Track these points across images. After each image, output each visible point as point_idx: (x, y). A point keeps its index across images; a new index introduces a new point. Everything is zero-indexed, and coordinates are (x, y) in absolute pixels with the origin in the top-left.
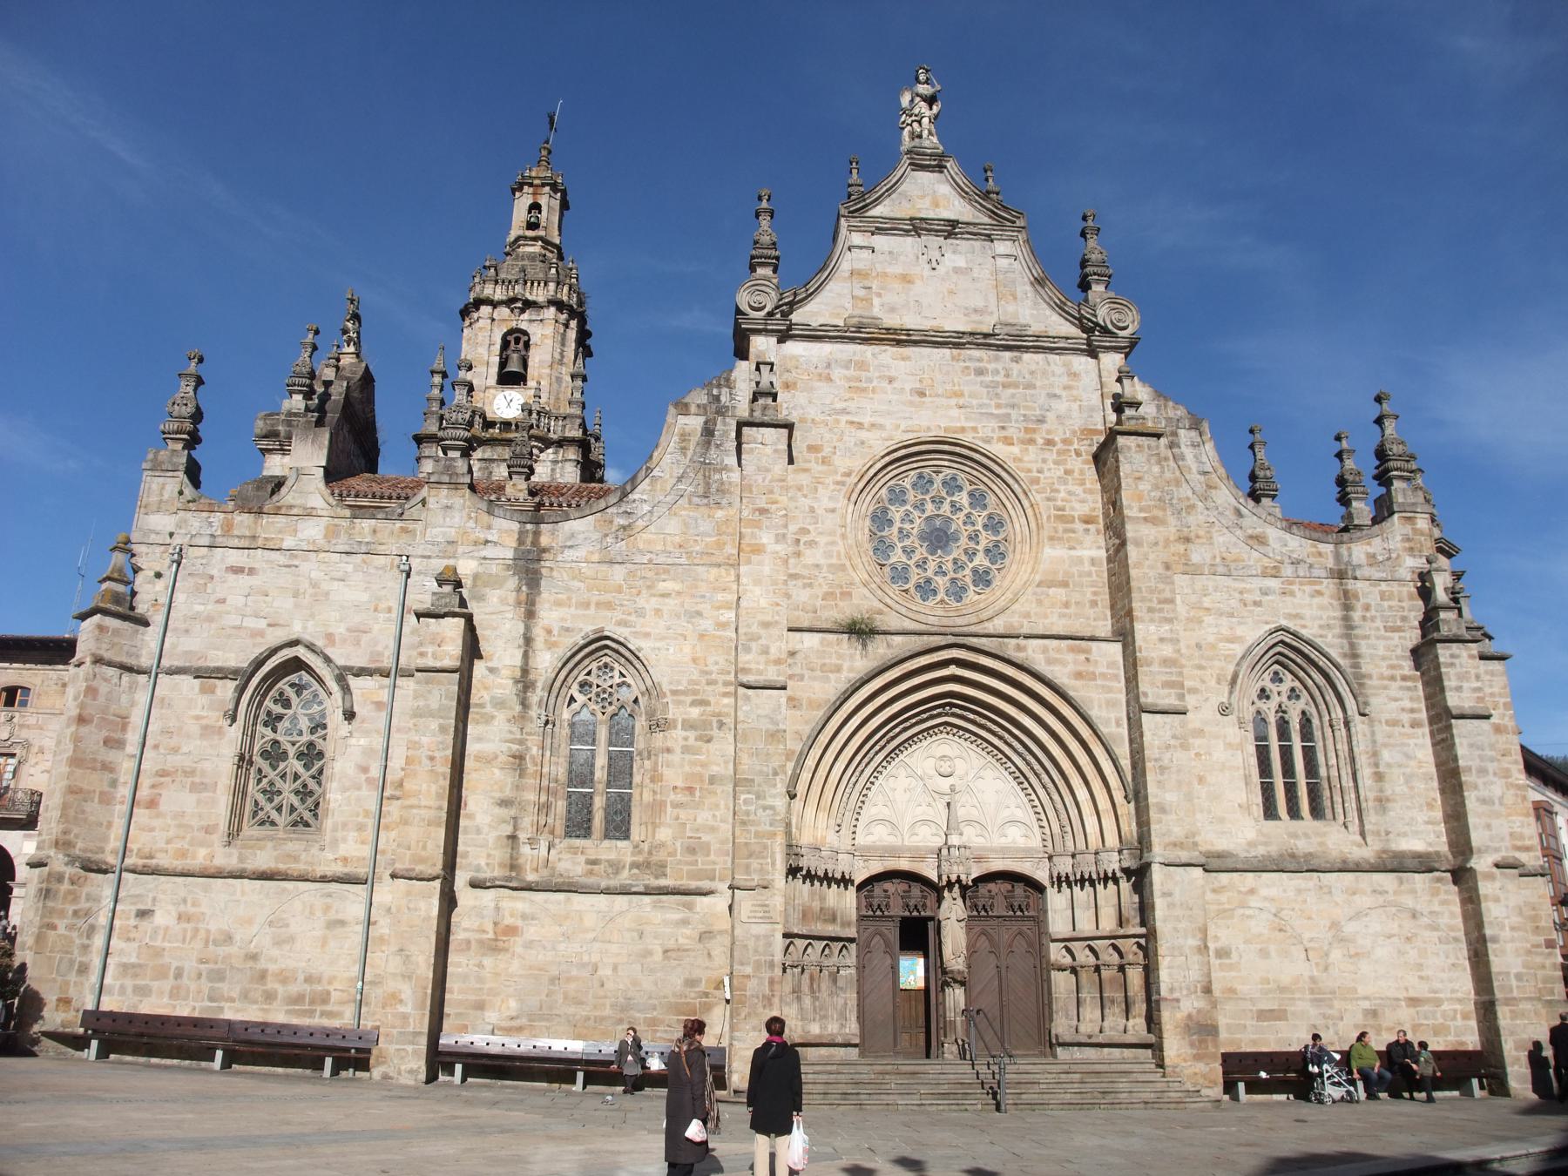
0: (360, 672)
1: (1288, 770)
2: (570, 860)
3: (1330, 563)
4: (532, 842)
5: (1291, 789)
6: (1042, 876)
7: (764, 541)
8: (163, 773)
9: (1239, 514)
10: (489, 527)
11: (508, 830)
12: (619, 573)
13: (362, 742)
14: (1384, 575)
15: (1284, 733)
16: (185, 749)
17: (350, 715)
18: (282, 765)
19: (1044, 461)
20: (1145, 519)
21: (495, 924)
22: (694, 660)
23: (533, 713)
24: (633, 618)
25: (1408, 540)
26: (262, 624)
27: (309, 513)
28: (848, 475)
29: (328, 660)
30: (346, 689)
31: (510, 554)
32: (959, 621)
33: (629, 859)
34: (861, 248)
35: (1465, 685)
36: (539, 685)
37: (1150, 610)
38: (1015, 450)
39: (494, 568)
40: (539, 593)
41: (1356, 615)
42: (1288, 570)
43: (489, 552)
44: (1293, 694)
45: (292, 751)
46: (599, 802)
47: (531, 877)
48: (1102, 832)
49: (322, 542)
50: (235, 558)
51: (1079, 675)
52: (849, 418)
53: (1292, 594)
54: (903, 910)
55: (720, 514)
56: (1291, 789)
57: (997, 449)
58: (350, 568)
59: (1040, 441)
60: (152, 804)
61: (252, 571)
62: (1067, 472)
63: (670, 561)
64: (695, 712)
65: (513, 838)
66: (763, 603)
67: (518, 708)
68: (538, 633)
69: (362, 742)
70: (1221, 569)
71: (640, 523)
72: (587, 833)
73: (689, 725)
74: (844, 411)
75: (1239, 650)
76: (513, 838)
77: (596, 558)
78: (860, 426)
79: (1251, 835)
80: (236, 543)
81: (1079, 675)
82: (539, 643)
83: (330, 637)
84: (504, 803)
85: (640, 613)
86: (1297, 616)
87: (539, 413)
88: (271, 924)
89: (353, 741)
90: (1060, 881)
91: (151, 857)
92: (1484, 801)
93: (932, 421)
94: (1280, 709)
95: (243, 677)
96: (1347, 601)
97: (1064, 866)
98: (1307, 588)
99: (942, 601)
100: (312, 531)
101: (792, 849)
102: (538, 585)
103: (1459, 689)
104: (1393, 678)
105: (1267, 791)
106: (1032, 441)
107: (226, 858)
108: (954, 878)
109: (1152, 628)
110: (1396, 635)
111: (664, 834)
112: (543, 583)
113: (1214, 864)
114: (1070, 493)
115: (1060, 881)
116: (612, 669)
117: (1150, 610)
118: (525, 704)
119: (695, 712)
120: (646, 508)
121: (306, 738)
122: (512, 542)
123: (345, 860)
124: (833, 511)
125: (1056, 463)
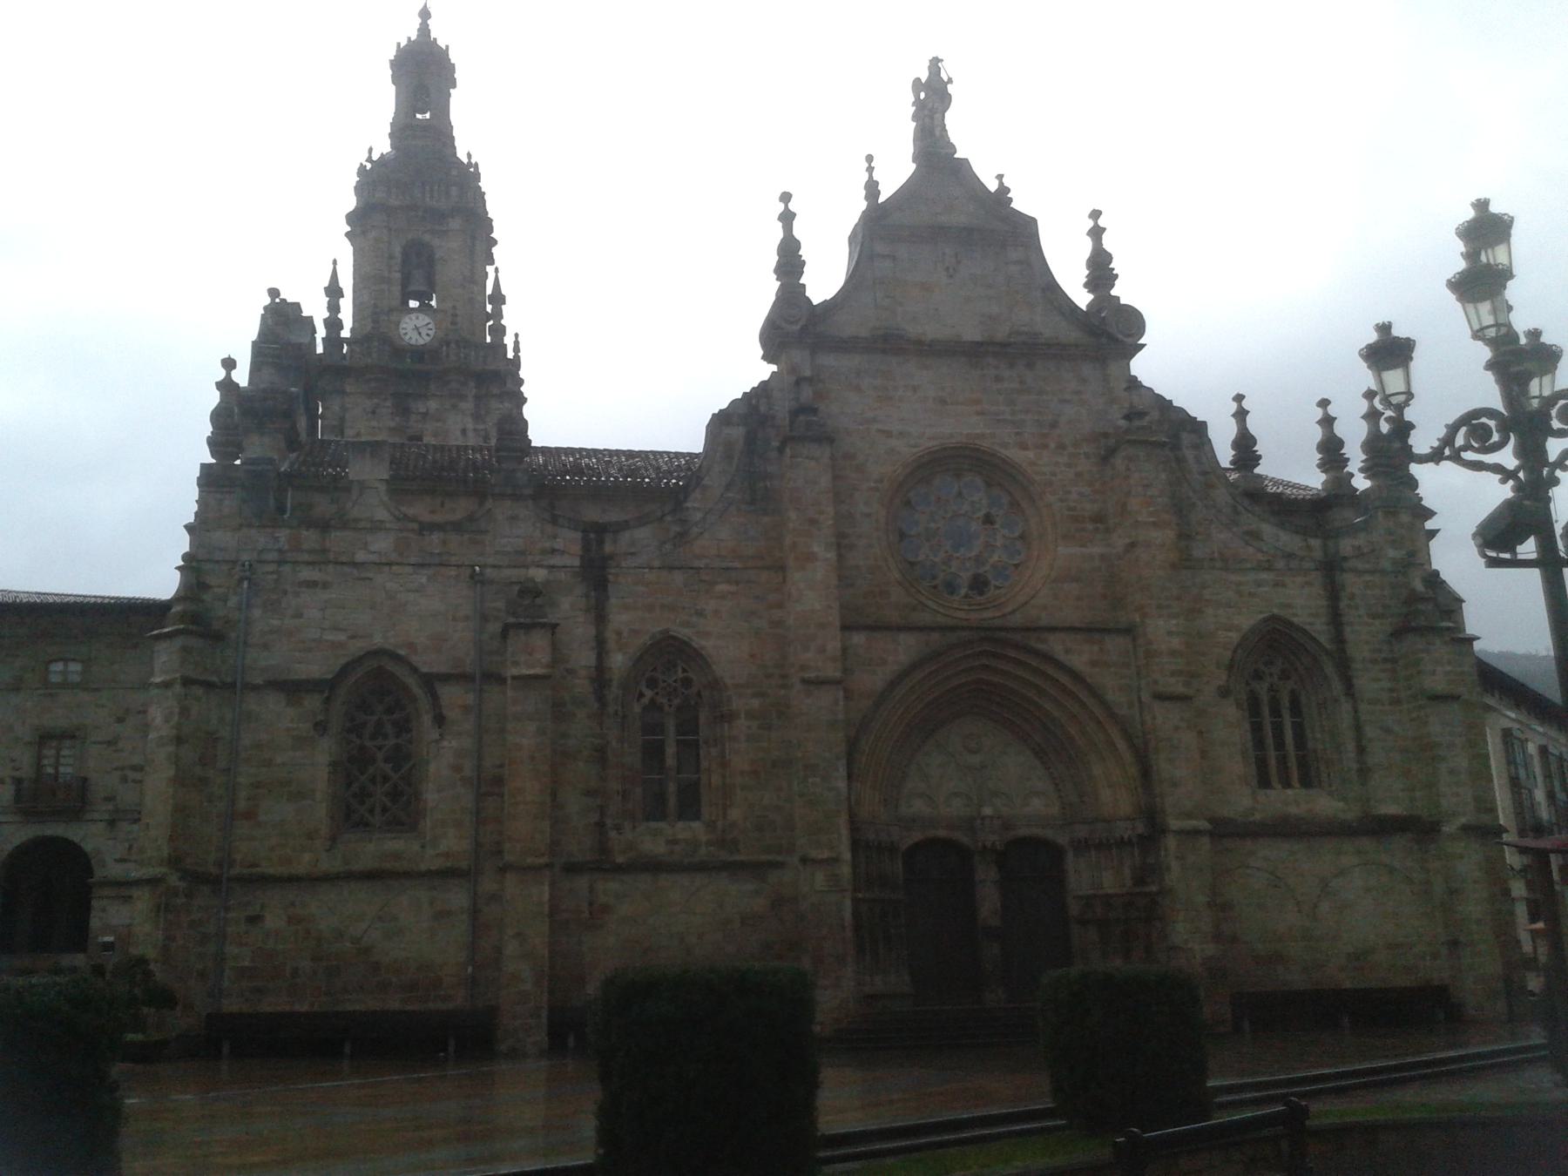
0: (446, 678)
1: (1280, 745)
2: (652, 840)
3: (1318, 554)
4: (618, 828)
5: (1283, 760)
6: (1062, 839)
7: (816, 549)
8: (257, 785)
9: (1236, 512)
10: (555, 537)
11: (595, 817)
12: (678, 578)
13: (454, 743)
14: (1367, 566)
15: (1276, 712)
16: (279, 760)
17: (440, 720)
18: (371, 770)
19: (1057, 463)
20: (1154, 524)
21: (591, 904)
22: (752, 656)
23: (611, 709)
24: (694, 619)
25: (1391, 534)
26: (342, 637)
27: (376, 527)
28: (881, 481)
29: (415, 670)
30: (434, 696)
31: (577, 562)
32: (987, 614)
33: (704, 838)
34: (884, 256)
35: (1439, 669)
36: (615, 683)
37: (1159, 607)
38: (1031, 454)
39: (562, 575)
40: (608, 598)
41: (1343, 604)
42: (1280, 564)
43: (556, 560)
44: (1285, 676)
45: (380, 756)
46: (672, 788)
47: (620, 859)
48: (1114, 797)
49: (394, 557)
50: (306, 574)
51: (1094, 664)
52: (880, 426)
53: (1284, 585)
54: (939, 864)
55: (766, 519)
56: (1283, 760)
57: (1014, 454)
58: (424, 580)
59: (1052, 445)
60: (250, 815)
61: (325, 586)
62: (1078, 475)
63: (724, 565)
64: (756, 703)
65: (600, 825)
66: (817, 606)
67: (596, 705)
68: (610, 636)
69: (454, 743)
70: (1219, 564)
71: (695, 530)
72: (663, 817)
73: (750, 715)
74: (874, 420)
75: (1235, 637)
76: (600, 825)
77: (657, 563)
78: (889, 434)
79: (1247, 802)
80: (306, 557)
81: (1094, 664)
82: (611, 644)
83: (411, 646)
84: (588, 793)
85: (700, 614)
86: (1289, 606)
87: (457, 342)
88: (380, 918)
89: (445, 743)
90: (1081, 846)
91: (257, 866)
92: (1452, 772)
93: (959, 426)
94: (1271, 689)
95: (326, 687)
96: (1334, 593)
97: (1082, 831)
98: (1299, 579)
99: (966, 596)
100: (382, 544)
101: (854, 827)
102: (605, 588)
103: (1434, 673)
104: (1374, 661)
105: (1262, 764)
106: (1046, 446)
107: (327, 864)
108: (988, 844)
109: (1161, 623)
110: (1377, 622)
111: (735, 814)
112: (610, 587)
113: (1224, 831)
114: (1080, 494)
115: (1081, 846)
116: (675, 666)
117: (1159, 607)
118: (601, 699)
119: (756, 703)
120: (699, 515)
121: (392, 742)
122: (577, 548)
123: (447, 855)
124: (868, 515)
125: (1069, 465)
